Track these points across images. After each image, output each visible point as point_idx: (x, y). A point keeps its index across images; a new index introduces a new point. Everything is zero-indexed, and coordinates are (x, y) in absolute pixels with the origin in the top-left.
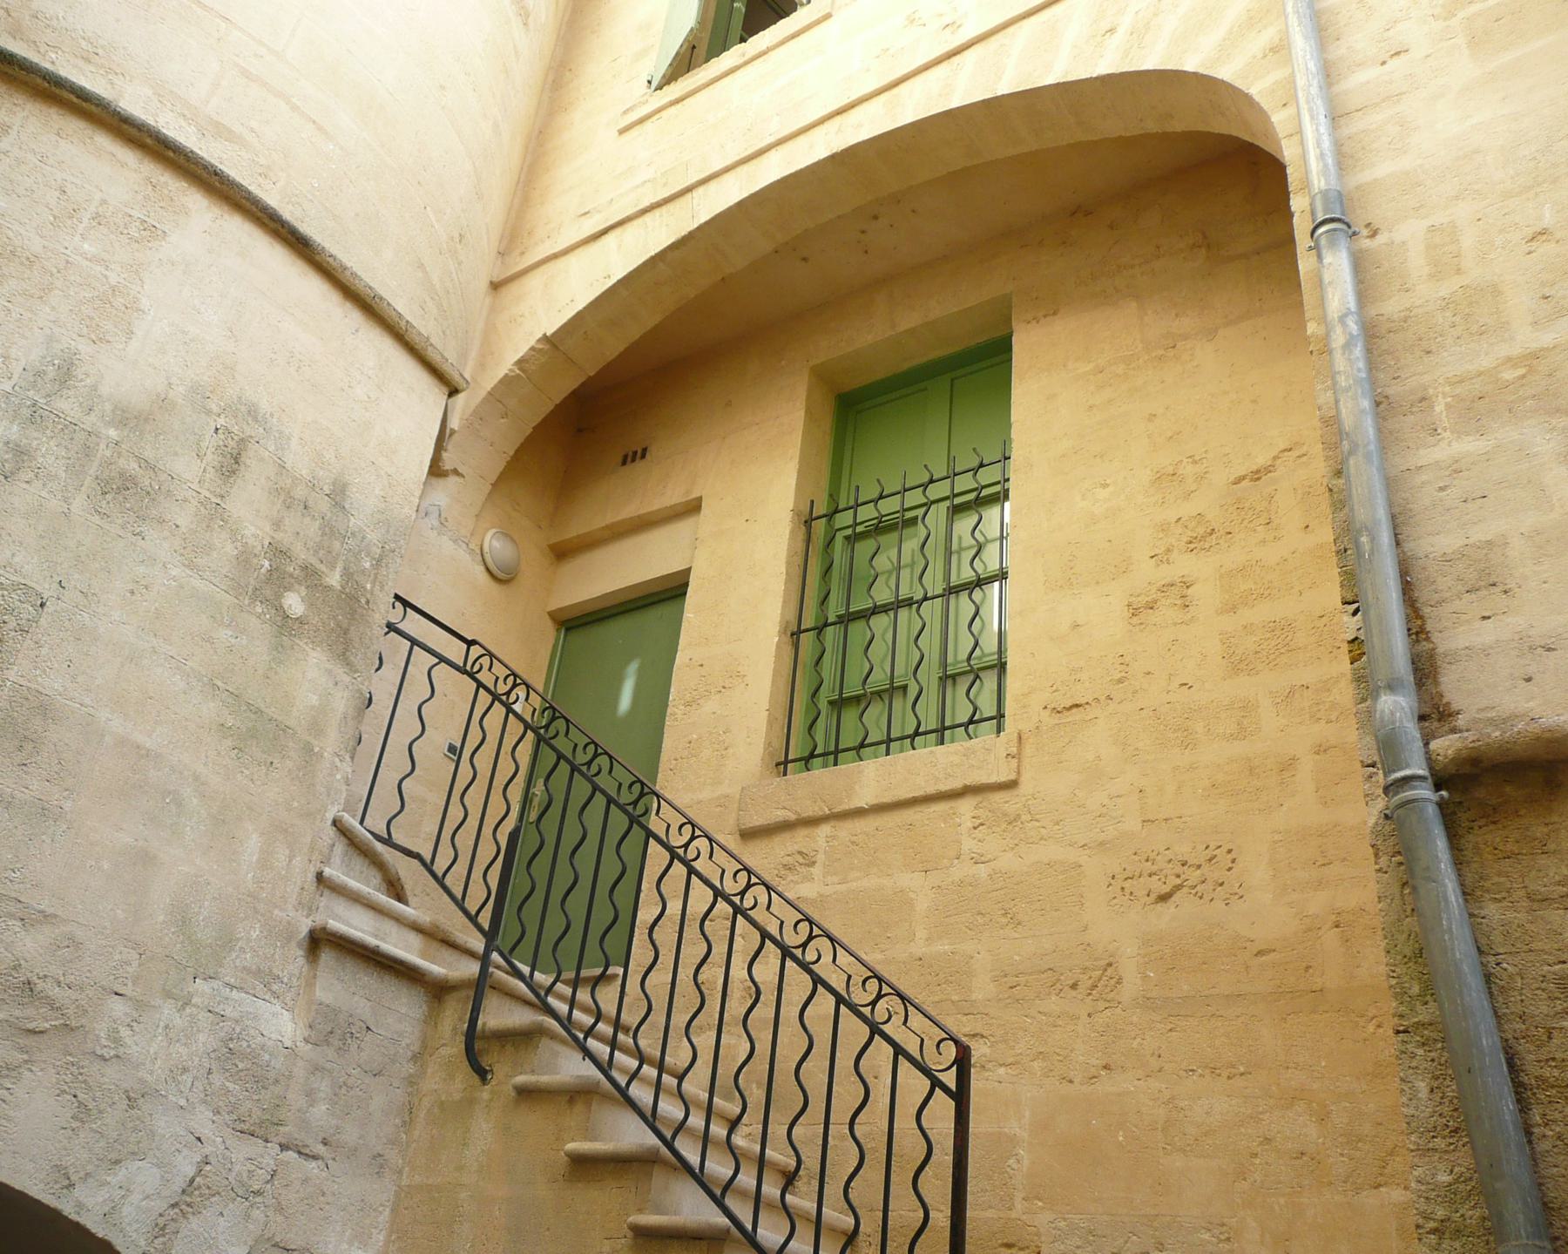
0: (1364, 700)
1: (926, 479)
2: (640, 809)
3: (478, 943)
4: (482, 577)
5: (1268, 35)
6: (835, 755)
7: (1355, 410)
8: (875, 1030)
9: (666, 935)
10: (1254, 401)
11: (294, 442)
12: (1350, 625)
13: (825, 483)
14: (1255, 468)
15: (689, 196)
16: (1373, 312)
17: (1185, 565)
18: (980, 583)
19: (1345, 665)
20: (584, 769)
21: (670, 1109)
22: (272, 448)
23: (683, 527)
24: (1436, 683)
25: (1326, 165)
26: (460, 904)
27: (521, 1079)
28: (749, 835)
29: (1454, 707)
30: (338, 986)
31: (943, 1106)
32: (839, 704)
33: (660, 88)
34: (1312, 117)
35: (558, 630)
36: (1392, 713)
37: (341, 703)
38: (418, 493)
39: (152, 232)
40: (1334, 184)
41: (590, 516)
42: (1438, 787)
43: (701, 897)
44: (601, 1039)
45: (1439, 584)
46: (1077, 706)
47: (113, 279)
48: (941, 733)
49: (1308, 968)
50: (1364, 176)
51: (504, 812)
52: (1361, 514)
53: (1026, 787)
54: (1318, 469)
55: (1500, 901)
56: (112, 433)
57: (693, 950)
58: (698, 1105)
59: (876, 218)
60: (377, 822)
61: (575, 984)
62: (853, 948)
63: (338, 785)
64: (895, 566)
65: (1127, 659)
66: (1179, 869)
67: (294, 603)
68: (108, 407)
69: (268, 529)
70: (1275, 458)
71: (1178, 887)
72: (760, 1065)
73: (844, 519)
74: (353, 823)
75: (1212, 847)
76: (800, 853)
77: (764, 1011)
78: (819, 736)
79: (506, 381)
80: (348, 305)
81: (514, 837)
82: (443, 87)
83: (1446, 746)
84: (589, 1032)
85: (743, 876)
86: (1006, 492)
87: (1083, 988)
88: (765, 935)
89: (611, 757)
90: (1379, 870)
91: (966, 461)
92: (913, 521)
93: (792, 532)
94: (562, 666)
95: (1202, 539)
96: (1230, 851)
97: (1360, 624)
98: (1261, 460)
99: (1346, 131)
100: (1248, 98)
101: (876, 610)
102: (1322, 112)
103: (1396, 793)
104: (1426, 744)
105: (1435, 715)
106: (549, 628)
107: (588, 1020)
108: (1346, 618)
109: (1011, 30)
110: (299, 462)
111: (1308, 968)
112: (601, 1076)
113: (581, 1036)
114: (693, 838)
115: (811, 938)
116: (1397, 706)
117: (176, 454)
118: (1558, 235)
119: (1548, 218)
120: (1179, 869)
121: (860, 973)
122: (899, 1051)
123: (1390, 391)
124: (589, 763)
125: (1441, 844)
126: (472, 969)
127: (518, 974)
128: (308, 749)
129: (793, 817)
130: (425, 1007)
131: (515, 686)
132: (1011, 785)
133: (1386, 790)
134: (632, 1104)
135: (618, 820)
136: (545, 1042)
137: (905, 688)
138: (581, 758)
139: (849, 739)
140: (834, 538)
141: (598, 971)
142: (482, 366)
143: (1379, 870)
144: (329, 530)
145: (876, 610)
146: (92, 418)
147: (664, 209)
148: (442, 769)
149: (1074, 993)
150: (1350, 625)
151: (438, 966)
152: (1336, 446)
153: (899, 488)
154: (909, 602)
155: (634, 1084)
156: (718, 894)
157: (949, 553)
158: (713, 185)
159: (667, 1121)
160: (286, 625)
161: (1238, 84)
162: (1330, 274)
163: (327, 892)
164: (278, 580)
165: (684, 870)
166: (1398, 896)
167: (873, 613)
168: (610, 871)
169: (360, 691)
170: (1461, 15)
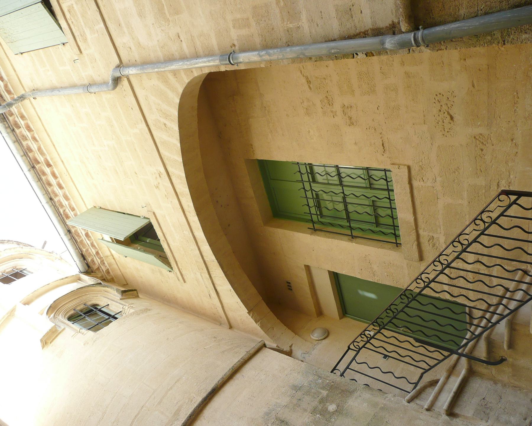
0: (387, 52)
1: (303, 190)
2: (410, 296)
3: (455, 357)
5: (170, 76)
6: (395, 227)
7: (290, 53)
8: (494, 222)
9: (456, 291)
10: (284, 82)
11: (278, 401)
12: (361, 56)
13: (302, 223)
14: (306, 83)
17: (337, 107)
18: (339, 174)
19: (375, 58)
20: (395, 314)
21: (519, 295)
22: (280, 409)
23: (314, 272)
24: (383, 28)
25: (212, 60)
26: (440, 361)
27: (505, 347)
28: (421, 258)
29: (391, 23)
30: (468, 407)
31: (523, 201)
32: (377, 224)
33: (172, 268)
34: (197, 64)
35: (346, 317)
36: (392, 44)
37: (367, 395)
38: (297, 361)
40: (218, 58)
41: (309, 303)
42: (418, 29)
43: (442, 278)
44: (491, 317)
45: (350, 27)
46: (383, 144)
49: (479, 70)
50: (216, 48)
51: (407, 343)
52: (324, 52)
53: (410, 163)
54: (309, 65)
55: (459, 9)
57: (461, 282)
58: (518, 286)
59: (217, 202)
60: (409, 387)
61: (471, 324)
62: (463, 228)
63: (395, 400)
64: (332, 202)
65: (368, 127)
66: (442, 112)
67: (332, 407)
69: (306, 414)
70: (303, 76)
71: (448, 113)
72: (504, 263)
73: (315, 218)
74: (409, 396)
75: (435, 101)
76: (429, 241)
77: (485, 260)
79: (262, 327)
80: (234, 378)
81: (417, 340)
82: (168, 339)
83: (404, 27)
84: (489, 321)
85: (436, 263)
86: (309, 164)
87: (482, 147)
88: (457, 257)
89: (391, 305)
90: (446, 49)
92: (317, 195)
93: (318, 236)
94: (359, 316)
95: (329, 101)
96: (436, 95)
97: (361, 53)
98: (304, 81)
99: (202, 53)
100: (189, 83)
101: (346, 209)
102: (195, 61)
103: (420, 43)
104: (403, 33)
105: (393, 29)
106: (345, 320)
107: (484, 321)
108: (359, 57)
109: (162, 156)
110: (285, 400)
111: (479, 70)
112: (506, 319)
113: (490, 324)
114: (421, 279)
115: (459, 242)
116: (389, 42)
120: (442, 112)
121: (473, 226)
122: (502, 215)
123: (285, 41)
124: (393, 312)
125: (438, 29)
126: (464, 360)
127: (466, 344)
128: (382, 409)
129: (416, 243)
130: (477, 378)
131: (364, 335)
132: (409, 168)
133: (418, 46)
134: (517, 309)
135: (414, 304)
136: (492, 337)
137: (373, 201)
138: (391, 314)
139: (389, 221)
140: (322, 222)
141: (467, 316)
142: (256, 335)
143: (446, 49)
144: (308, 393)
145: (346, 209)
147: (210, 270)
148: (393, 362)
149: (484, 150)
150: (361, 56)
151: (463, 372)
152: (301, 59)
153: (305, 199)
154: (344, 198)
155: (509, 307)
156: (442, 272)
158: (204, 254)
159: (524, 297)
160: (339, 411)
161: (184, 86)
162: (246, 59)
163: (433, 408)
164: (324, 412)
165: (433, 283)
166: (455, 43)
167: (347, 210)
168: (431, 308)
169: (363, 388)
170: (168, 17)
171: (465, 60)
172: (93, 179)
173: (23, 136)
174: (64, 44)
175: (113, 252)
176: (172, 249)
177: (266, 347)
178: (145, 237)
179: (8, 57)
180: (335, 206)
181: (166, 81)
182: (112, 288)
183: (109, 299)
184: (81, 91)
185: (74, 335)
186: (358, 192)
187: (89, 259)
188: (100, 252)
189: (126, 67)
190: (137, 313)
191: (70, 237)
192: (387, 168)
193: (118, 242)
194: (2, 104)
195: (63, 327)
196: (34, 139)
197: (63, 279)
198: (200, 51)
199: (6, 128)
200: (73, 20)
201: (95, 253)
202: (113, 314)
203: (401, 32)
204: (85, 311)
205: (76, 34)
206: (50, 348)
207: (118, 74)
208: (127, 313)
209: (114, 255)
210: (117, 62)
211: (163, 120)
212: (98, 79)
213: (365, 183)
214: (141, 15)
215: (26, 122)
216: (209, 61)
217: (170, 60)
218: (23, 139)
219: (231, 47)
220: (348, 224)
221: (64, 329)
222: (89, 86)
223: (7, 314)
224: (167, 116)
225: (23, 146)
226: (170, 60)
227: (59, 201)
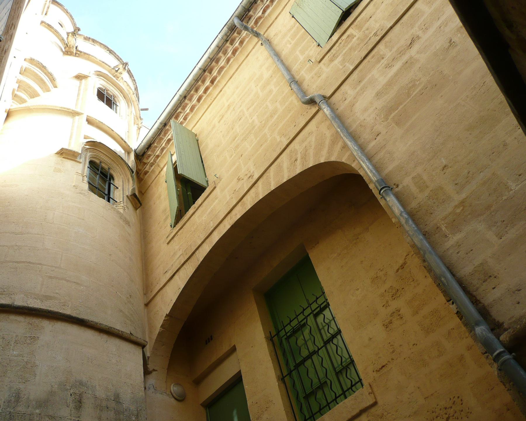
0: (471, 331)
1: (302, 310)
4: (173, 400)
5: (340, 144)
7: (419, 240)
11: (97, 387)
14: (400, 265)
15: (195, 254)
16: (409, 209)
17: (395, 305)
18: (334, 336)
23: (233, 357)
24: (491, 316)
25: (374, 173)
29: (501, 321)
33: (174, 226)
34: (363, 162)
36: (482, 333)
39: (34, 339)
40: (379, 177)
42: (510, 353)
46: (383, 366)
47: (25, 359)
48: (344, 394)
50: (386, 171)
52: (438, 271)
53: (380, 403)
56: (38, 411)
64: (306, 341)
68: (34, 403)
70: (405, 259)
73: (282, 333)
75: (452, 398)
78: (306, 413)
79: (160, 334)
82: (110, 255)
83: (504, 337)
90: (508, 390)
91: (312, 299)
92: (305, 325)
93: (268, 345)
95: (395, 294)
96: (458, 397)
98: (401, 262)
99: (375, 161)
100: (343, 163)
101: (305, 360)
102: (365, 159)
103: (498, 360)
104: (499, 339)
105: (496, 327)
106: (202, 409)
108: (451, 306)
109: (268, 171)
110: (101, 393)
116: (481, 330)
117: (60, 409)
118: (450, 165)
119: (444, 162)
123: (426, 230)
132: (375, 404)
137: (326, 382)
139: (315, 409)
140: (282, 343)
142: (151, 332)
144: (118, 412)
145: (305, 360)
146: (30, 409)
150: (453, 307)
157: (320, 330)
158: (200, 249)
161: (338, 160)
162: (391, 202)
170: (390, 118)
171: (508, 410)
172: (219, 122)
173: (226, 51)
174: (319, 45)
175: (165, 169)
176: (191, 219)
177: (143, 348)
178: (190, 191)
179: (284, 7)
180: (303, 346)
181: (333, 143)
182: (133, 183)
183: (123, 186)
184: (288, 77)
185: (77, 174)
186: (327, 363)
187: (149, 153)
188: (159, 158)
189: (327, 104)
190: (121, 216)
191: (160, 128)
192: (364, 381)
193: (175, 169)
194: (244, 23)
195: (81, 161)
196: (228, 60)
197: (122, 139)
198: (376, 159)
199: (226, 34)
200: (343, 43)
201: (157, 154)
202: (111, 196)
203: (498, 337)
204: (103, 171)
205: (332, 51)
206: (59, 159)
207: (318, 100)
208: (117, 208)
209: (163, 171)
210: (328, 94)
211: (299, 156)
212: (305, 85)
213: (338, 366)
214: (379, 95)
215: (239, 47)
216: (371, 171)
217: (354, 137)
218: (223, 51)
219: (395, 184)
220: (292, 368)
221: (80, 163)
222: (295, 82)
223: (73, 110)
224: (304, 157)
225: (217, 55)
226: (354, 137)
227: (187, 104)
